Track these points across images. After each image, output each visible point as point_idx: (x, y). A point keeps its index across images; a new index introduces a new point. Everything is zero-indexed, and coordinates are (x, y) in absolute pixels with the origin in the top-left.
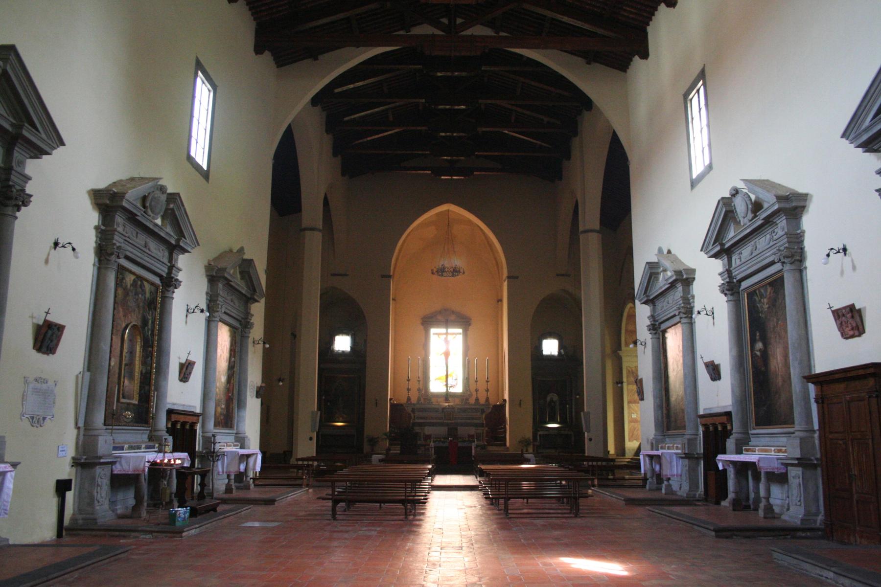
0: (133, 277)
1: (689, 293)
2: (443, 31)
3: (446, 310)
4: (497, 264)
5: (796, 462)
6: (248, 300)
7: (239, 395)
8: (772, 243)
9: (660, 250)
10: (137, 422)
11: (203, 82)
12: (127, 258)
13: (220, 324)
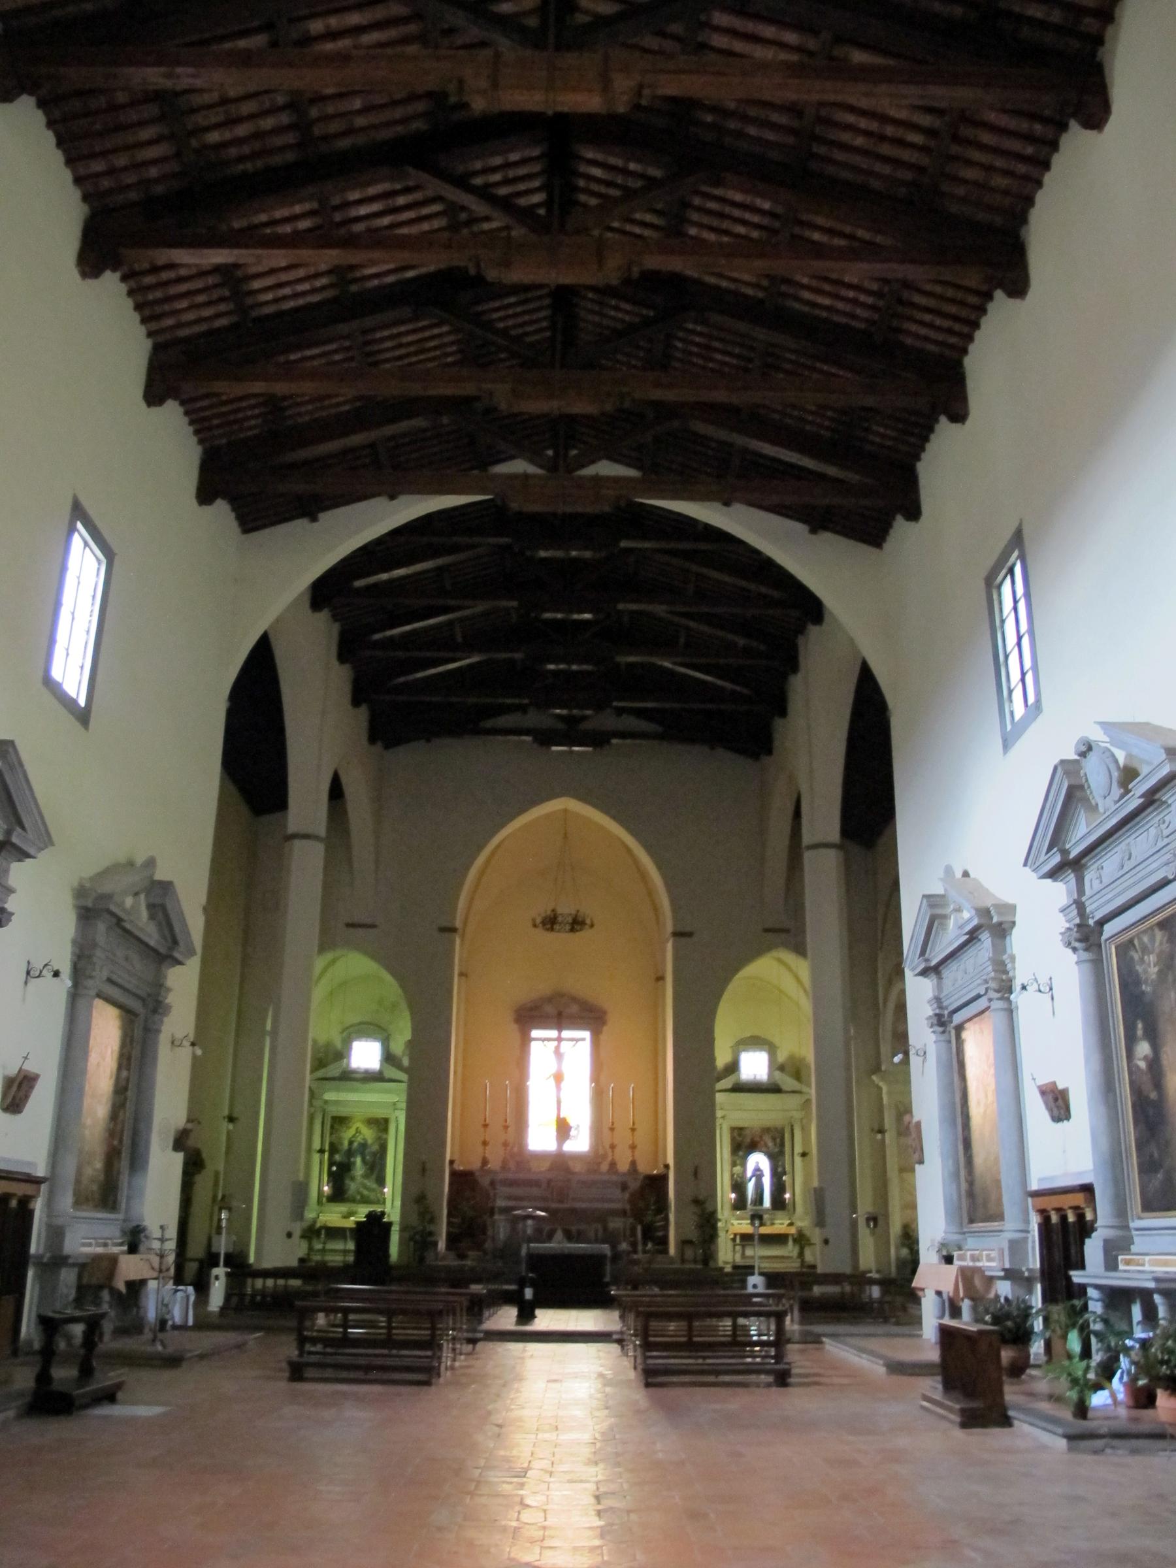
1: (1004, 951)
2: (541, 467)
4: (656, 909)
6: (165, 956)
8: (1160, 844)
9: (949, 870)
11: (86, 544)
13: (99, 1004)
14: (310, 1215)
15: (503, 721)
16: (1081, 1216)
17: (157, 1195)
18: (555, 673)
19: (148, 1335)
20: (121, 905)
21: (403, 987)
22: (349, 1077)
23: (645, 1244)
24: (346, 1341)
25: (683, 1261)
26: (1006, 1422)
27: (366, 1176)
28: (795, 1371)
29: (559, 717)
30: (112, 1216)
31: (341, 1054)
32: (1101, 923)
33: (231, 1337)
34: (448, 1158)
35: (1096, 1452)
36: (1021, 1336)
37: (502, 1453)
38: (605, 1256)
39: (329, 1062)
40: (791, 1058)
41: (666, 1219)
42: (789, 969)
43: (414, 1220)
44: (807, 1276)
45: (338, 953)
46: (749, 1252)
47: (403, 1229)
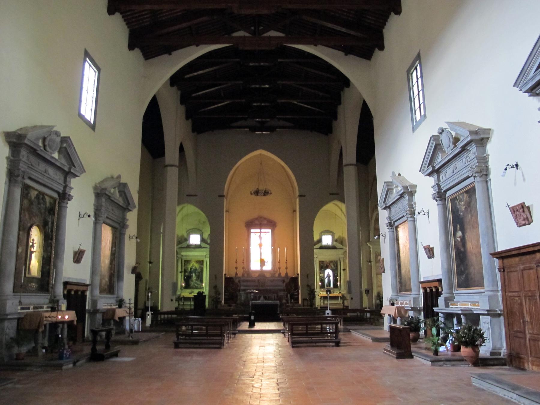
0: (36, 193)
2: (250, 33)
3: (261, 217)
5: (486, 312)
6: (126, 208)
8: (467, 164)
9: (393, 173)
11: (90, 66)
12: (30, 178)
13: (104, 225)
14: (178, 293)
15: (239, 123)
16: (437, 290)
17: (127, 288)
18: (257, 106)
19: (127, 334)
20: (110, 192)
21: (207, 216)
22: (189, 247)
23: (291, 300)
24: (193, 335)
25: (304, 306)
26: (412, 357)
27: (196, 280)
28: (341, 341)
29: (258, 121)
30: (112, 296)
31: (187, 239)
32: (446, 191)
33: (154, 334)
34: (224, 273)
35: (440, 366)
36: (417, 329)
37: (246, 370)
38: (278, 305)
39: (183, 241)
40: (340, 237)
41: (298, 292)
42: (338, 206)
43: (213, 295)
44: (346, 310)
45: (184, 205)
46: (326, 302)
47: (210, 297)
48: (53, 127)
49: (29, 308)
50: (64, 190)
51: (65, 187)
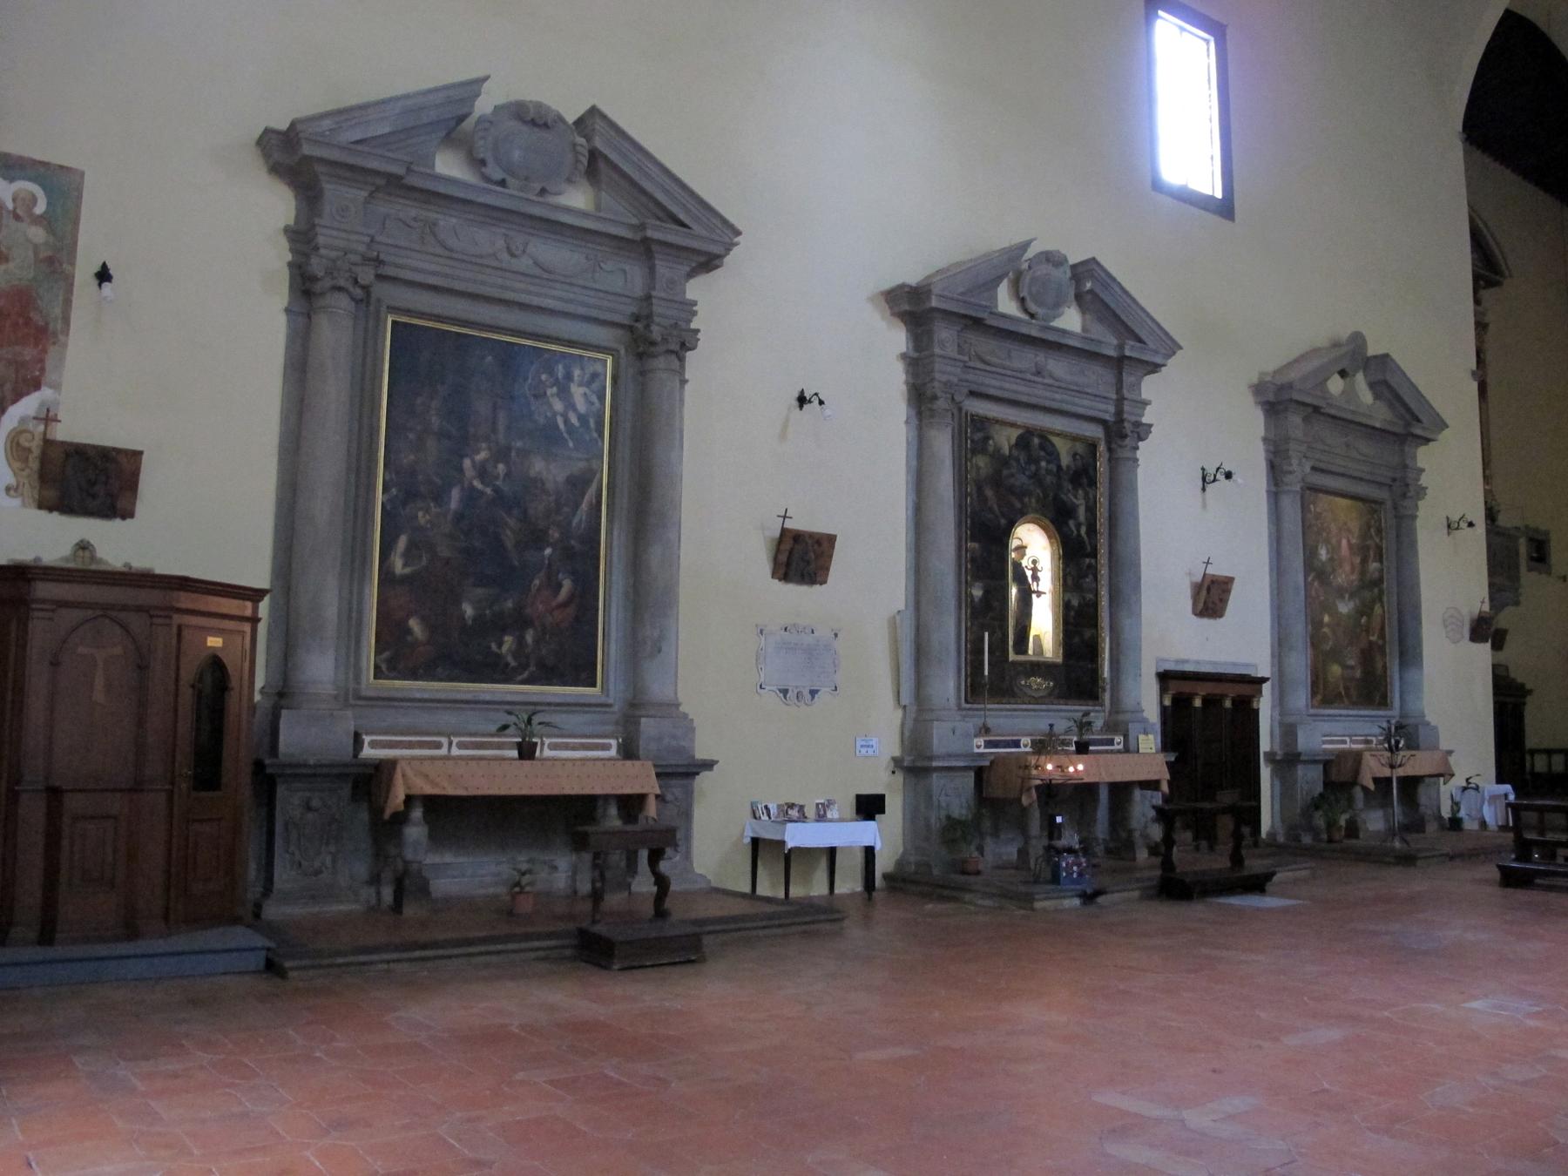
0: (1014, 434)
7: (1401, 641)
10: (1059, 697)
48: (1025, 246)
49: (1016, 744)
50: (1119, 412)
51: (1120, 400)
